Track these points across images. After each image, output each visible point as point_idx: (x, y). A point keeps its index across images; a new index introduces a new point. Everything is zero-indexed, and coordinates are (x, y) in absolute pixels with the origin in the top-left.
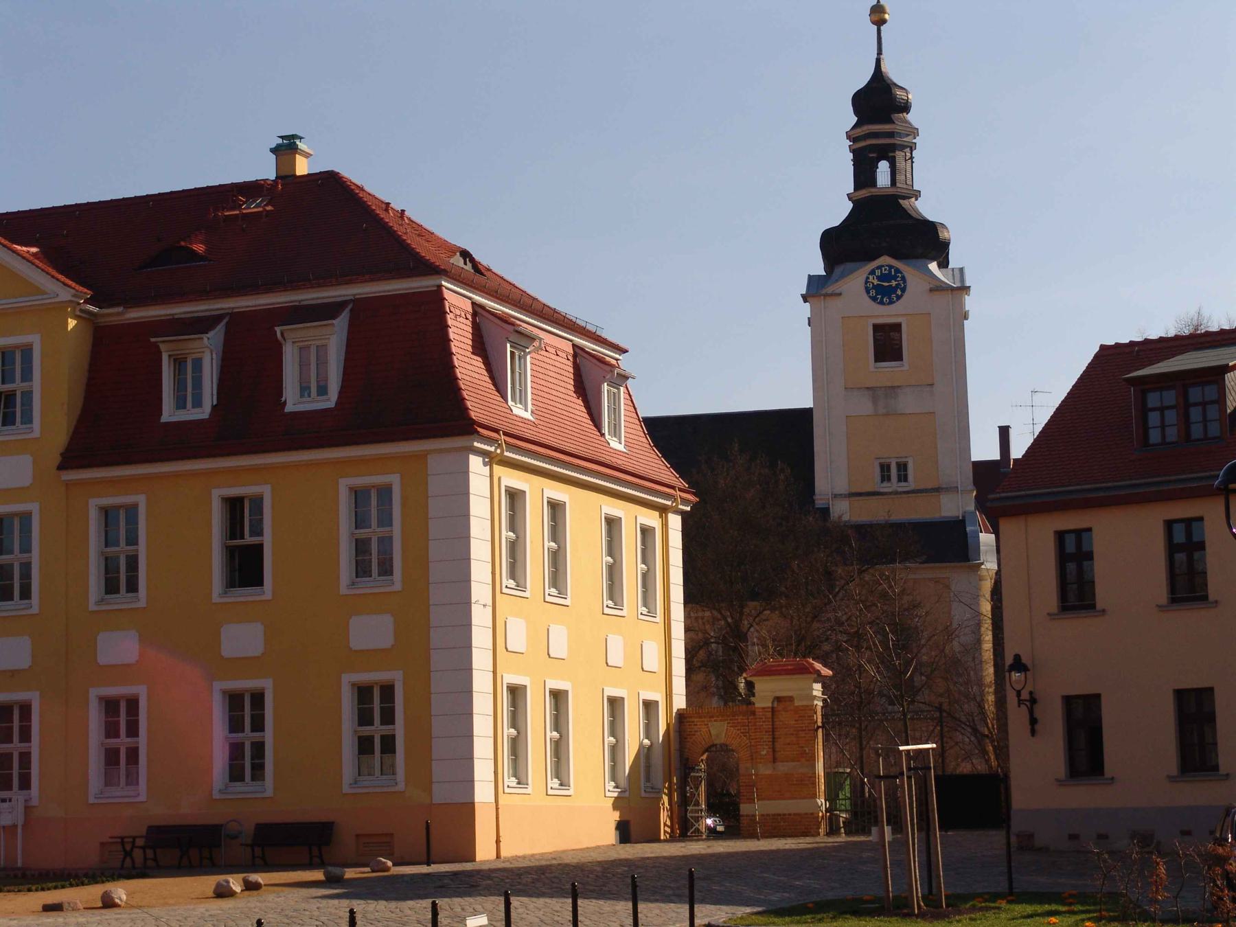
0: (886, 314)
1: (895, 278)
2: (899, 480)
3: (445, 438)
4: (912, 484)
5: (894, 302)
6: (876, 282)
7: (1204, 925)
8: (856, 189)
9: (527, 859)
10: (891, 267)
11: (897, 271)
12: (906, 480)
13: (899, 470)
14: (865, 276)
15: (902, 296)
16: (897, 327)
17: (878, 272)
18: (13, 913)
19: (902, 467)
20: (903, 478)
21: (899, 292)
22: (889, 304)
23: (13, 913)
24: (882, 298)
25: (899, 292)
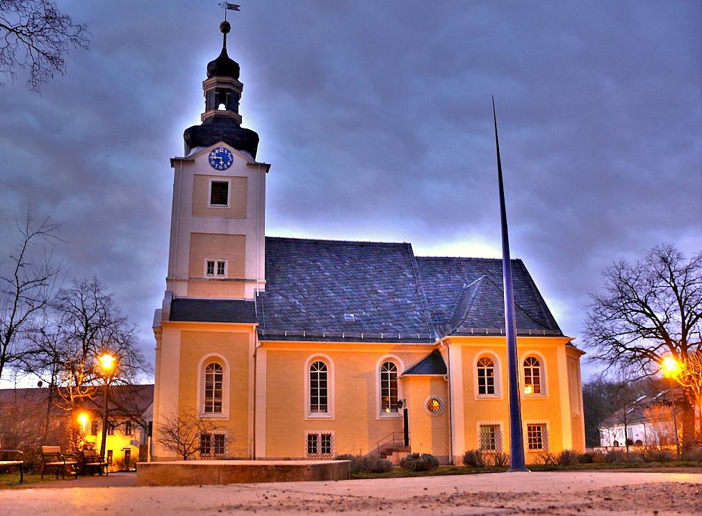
0: (220, 176)
1: (225, 163)
2: (219, 273)
3: (86, 478)
4: (226, 276)
5: (225, 169)
6: (215, 158)
7: (697, 414)
8: (209, 77)
9: (622, 507)
10: (225, 149)
11: (228, 151)
12: (223, 273)
13: (219, 267)
14: (208, 154)
15: (230, 166)
16: (225, 185)
17: (217, 151)
18: (284, 492)
19: (221, 265)
20: (221, 272)
21: (229, 163)
22: (222, 170)
23: (284, 492)
24: (218, 167)
25: (229, 163)
